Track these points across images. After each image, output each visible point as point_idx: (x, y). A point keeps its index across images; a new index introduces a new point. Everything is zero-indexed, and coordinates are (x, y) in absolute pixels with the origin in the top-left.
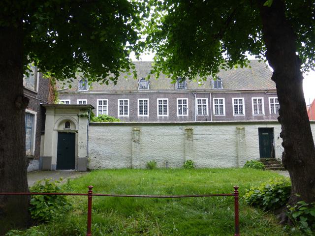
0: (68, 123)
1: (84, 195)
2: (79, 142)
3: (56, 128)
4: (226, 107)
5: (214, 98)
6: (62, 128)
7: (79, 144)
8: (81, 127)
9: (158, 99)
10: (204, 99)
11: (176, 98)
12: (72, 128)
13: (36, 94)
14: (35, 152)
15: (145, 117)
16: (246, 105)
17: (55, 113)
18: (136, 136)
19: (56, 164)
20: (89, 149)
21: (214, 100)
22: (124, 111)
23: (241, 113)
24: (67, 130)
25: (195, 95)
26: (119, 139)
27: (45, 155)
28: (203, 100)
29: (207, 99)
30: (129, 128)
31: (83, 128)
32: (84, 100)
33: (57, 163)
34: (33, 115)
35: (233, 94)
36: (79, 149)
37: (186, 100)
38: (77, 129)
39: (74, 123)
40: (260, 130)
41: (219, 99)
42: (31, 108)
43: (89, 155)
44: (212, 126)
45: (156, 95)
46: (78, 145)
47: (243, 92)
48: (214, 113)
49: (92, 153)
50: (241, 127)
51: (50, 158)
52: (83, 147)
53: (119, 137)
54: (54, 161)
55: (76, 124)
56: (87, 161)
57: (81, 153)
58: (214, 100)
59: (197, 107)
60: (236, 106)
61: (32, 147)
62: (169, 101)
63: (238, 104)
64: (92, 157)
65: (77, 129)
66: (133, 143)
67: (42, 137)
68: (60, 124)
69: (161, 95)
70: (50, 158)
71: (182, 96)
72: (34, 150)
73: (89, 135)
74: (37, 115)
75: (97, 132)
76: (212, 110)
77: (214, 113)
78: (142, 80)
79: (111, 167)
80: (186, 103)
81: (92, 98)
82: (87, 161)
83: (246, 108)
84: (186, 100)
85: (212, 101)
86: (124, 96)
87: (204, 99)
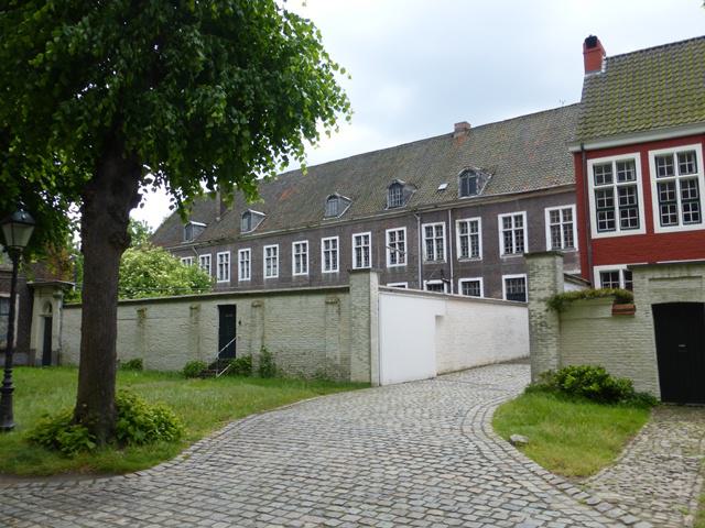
1: (513, 362)
4: (483, 238)
9: (354, 235)
10: (437, 224)
15: (400, 268)
16: (529, 228)
21: (457, 225)
22: (514, 244)
23: (476, 253)
29: (444, 224)
32: (401, 229)
35: (499, 204)
40: (221, 308)
41: (468, 220)
44: (166, 305)
47: (521, 197)
48: (459, 254)
50: (195, 304)
58: (457, 225)
59: (424, 243)
60: (508, 234)
63: (691, 212)
76: (448, 248)
77: (459, 254)
81: (257, 245)
83: (529, 238)
86: (302, 235)
87: (437, 224)
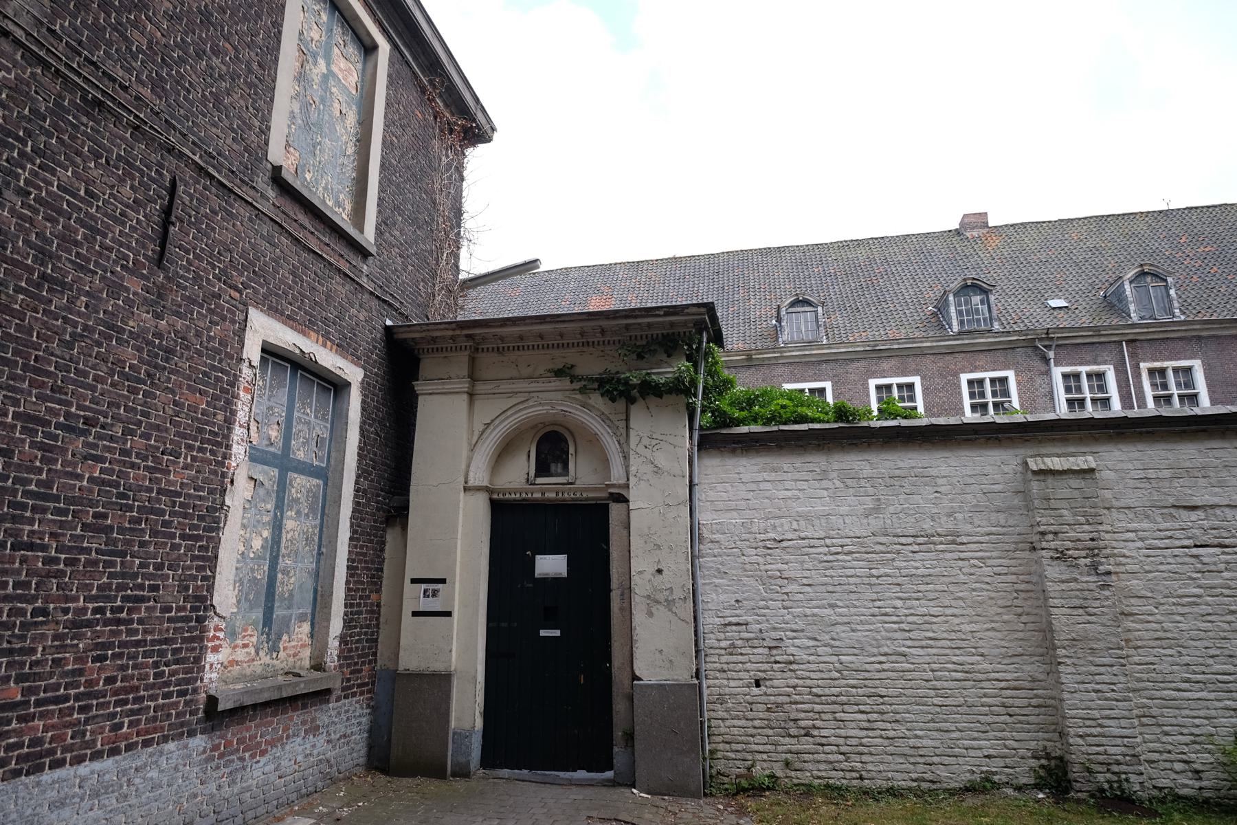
0: (552, 448)
2: (636, 566)
3: (479, 476)
5: (1144, 366)
6: (517, 476)
7: (641, 585)
8: (654, 476)
9: (873, 383)
11: (956, 375)
12: (581, 478)
13: (364, 253)
14: (343, 640)
17: (473, 378)
18: (1068, 516)
19: (479, 723)
20: (709, 621)
24: (550, 488)
25: (1051, 354)
26: (927, 539)
27: (409, 661)
28: (1089, 375)
30: (995, 466)
31: (657, 470)
33: (487, 714)
34: (336, 387)
36: (639, 617)
37: (1003, 380)
38: (617, 475)
39: (594, 440)
42: (327, 336)
43: (711, 664)
45: (861, 366)
46: (628, 590)
49: (732, 649)
51: (442, 681)
52: (669, 603)
53: (927, 525)
54: (467, 709)
55: (611, 444)
56: (687, 700)
57: (652, 649)
61: (327, 605)
62: (926, 390)
64: (726, 685)
65: (617, 475)
66: (1054, 571)
67: (391, 536)
68: (505, 451)
69: (886, 365)
70: (442, 681)
71: (982, 360)
72: (336, 626)
73: (704, 517)
74: (365, 386)
75: (751, 496)
78: (793, 304)
79: (900, 774)
80: (1006, 393)
82: (687, 700)
84: (1003, 380)
85: (1138, 375)
